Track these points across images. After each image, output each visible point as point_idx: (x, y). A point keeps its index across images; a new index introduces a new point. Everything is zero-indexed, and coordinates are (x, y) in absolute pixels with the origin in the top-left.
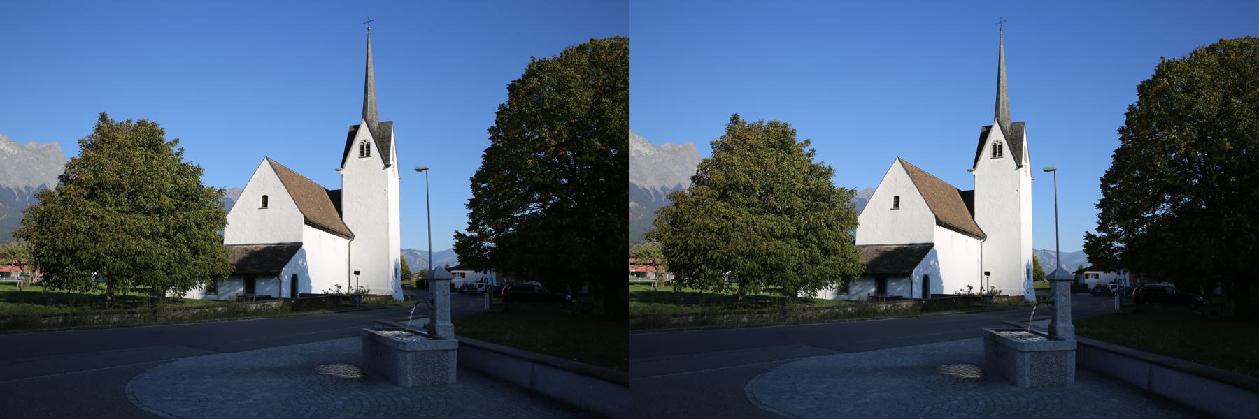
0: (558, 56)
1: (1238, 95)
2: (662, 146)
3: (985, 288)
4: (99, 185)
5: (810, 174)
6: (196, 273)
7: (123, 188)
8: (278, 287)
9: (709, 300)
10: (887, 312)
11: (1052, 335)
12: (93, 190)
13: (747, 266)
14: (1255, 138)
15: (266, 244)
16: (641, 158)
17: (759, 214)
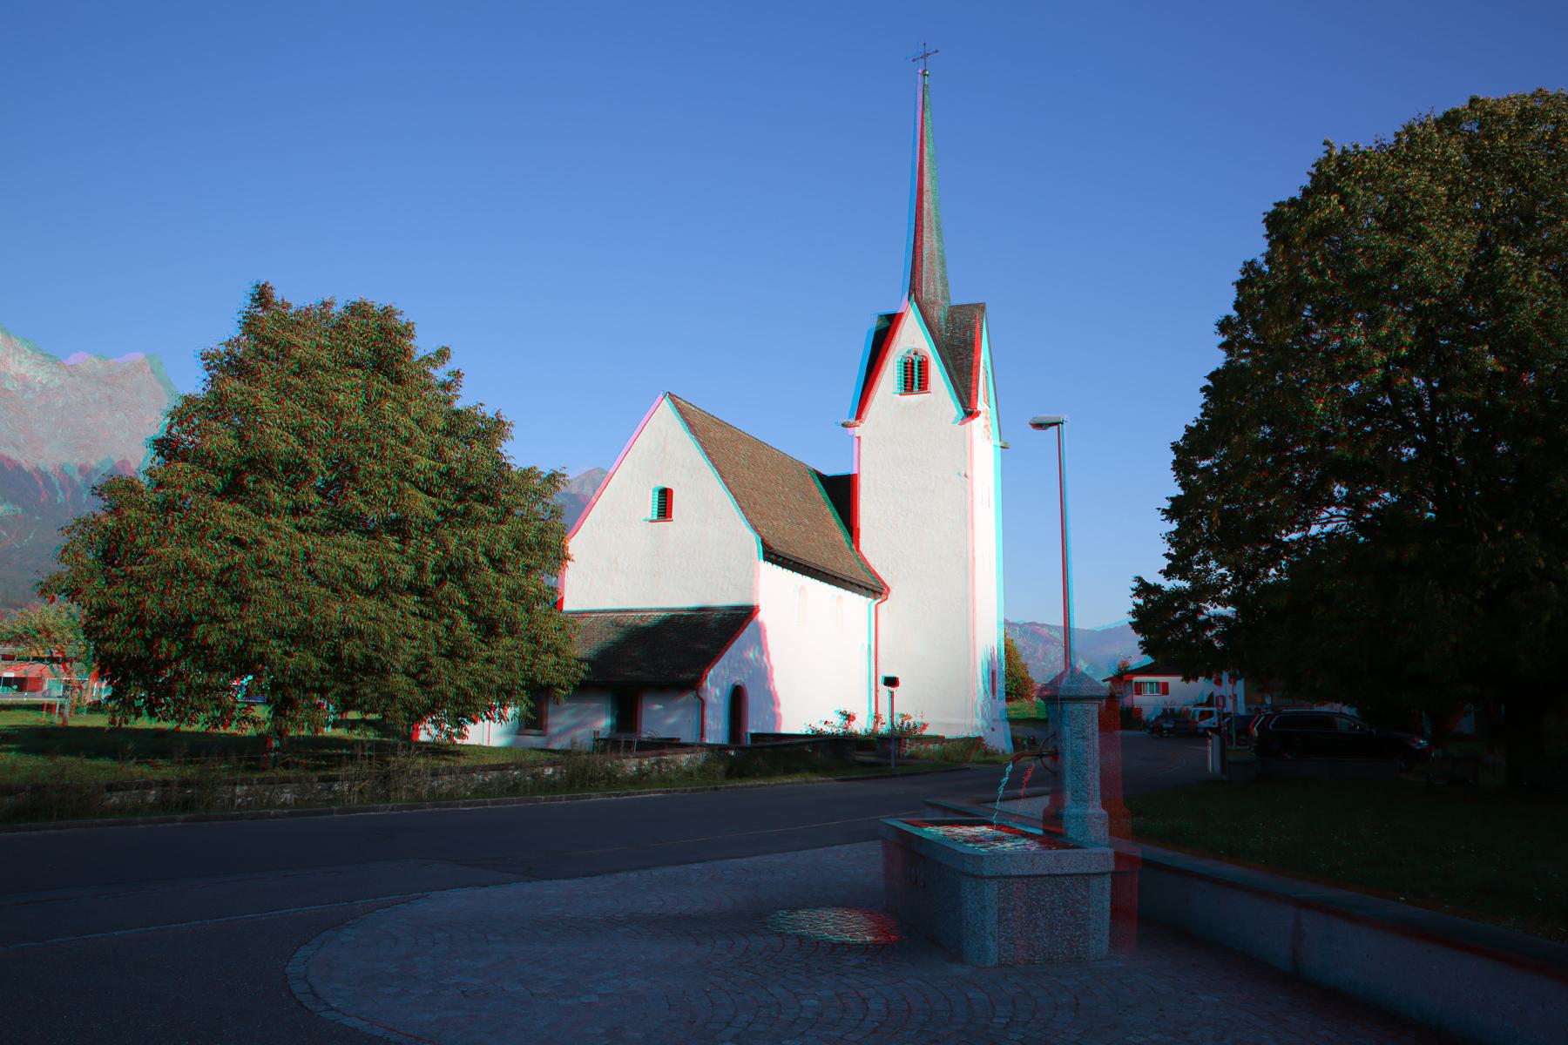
0: (1390, 140)
1: (1514, 236)
2: (65, 361)
3: (886, 718)
4: (251, 462)
5: (449, 434)
6: (492, 681)
7: (310, 473)
8: (695, 718)
9: (199, 748)
10: (641, 778)
11: (1054, 833)
12: (238, 474)
13: (292, 662)
14: (1558, 344)
16: (29, 396)
17: (322, 535)
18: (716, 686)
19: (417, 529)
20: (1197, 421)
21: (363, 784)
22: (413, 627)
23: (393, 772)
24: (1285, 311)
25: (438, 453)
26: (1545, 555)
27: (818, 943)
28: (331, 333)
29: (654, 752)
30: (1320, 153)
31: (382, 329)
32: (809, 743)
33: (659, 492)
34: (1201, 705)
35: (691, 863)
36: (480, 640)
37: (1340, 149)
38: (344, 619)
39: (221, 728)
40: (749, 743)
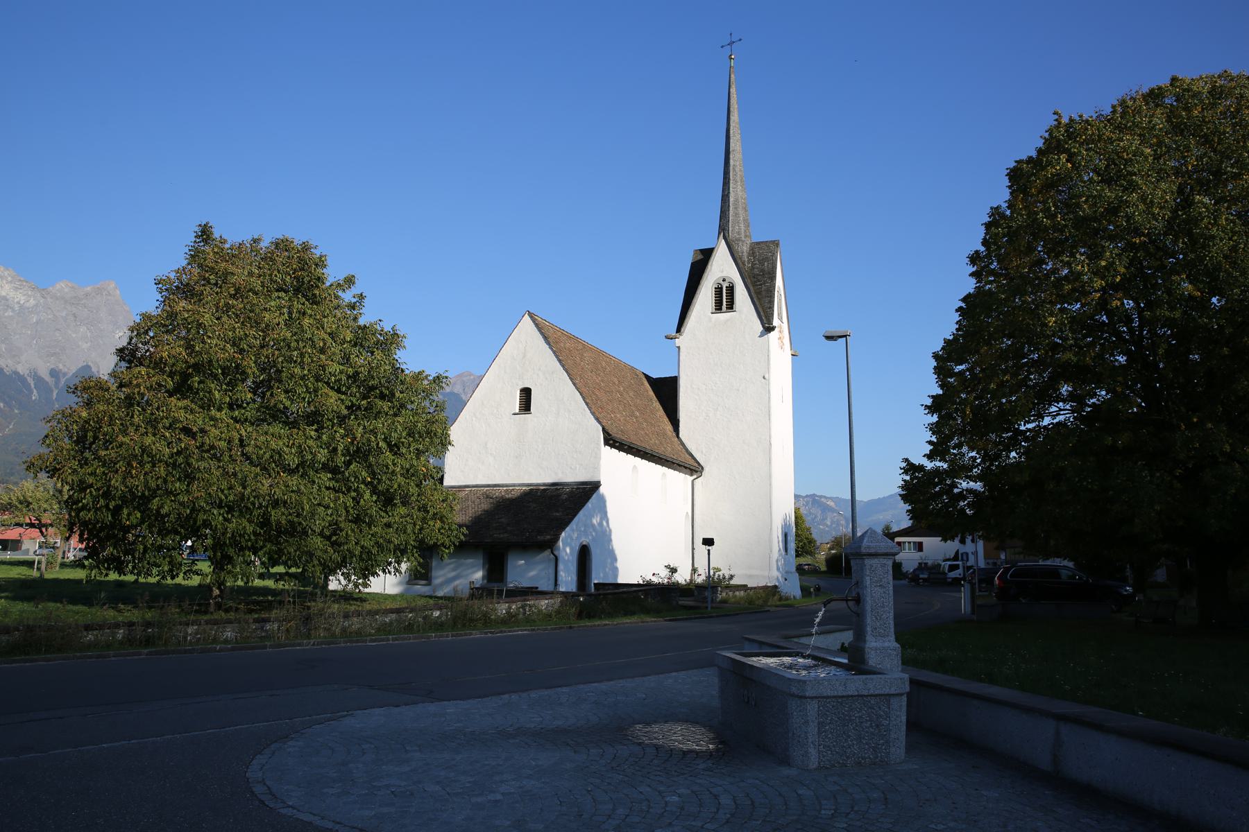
0: (1107, 110)
1: (1204, 186)
4: (197, 367)
6: (390, 542)
7: (244, 373)
8: (552, 571)
9: (159, 596)
10: (509, 620)
11: (856, 661)
12: (185, 377)
18: (567, 546)
19: (328, 420)
20: (954, 334)
21: (289, 624)
22: (327, 498)
23: (314, 614)
24: (1024, 246)
25: (346, 359)
26: (1230, 441)
27: (671, 751)
28: (260, 264)
29: (519, 598)
30: (1050, 121)
31: (300, 259)
32: (641, 591)
33: (521, 391)
34: (948, 560)
35: (560, 687)
36: (380, 509)
37: (1068, 118)
38: (271, 491)
39: (169, 578)
40: (593, 590)
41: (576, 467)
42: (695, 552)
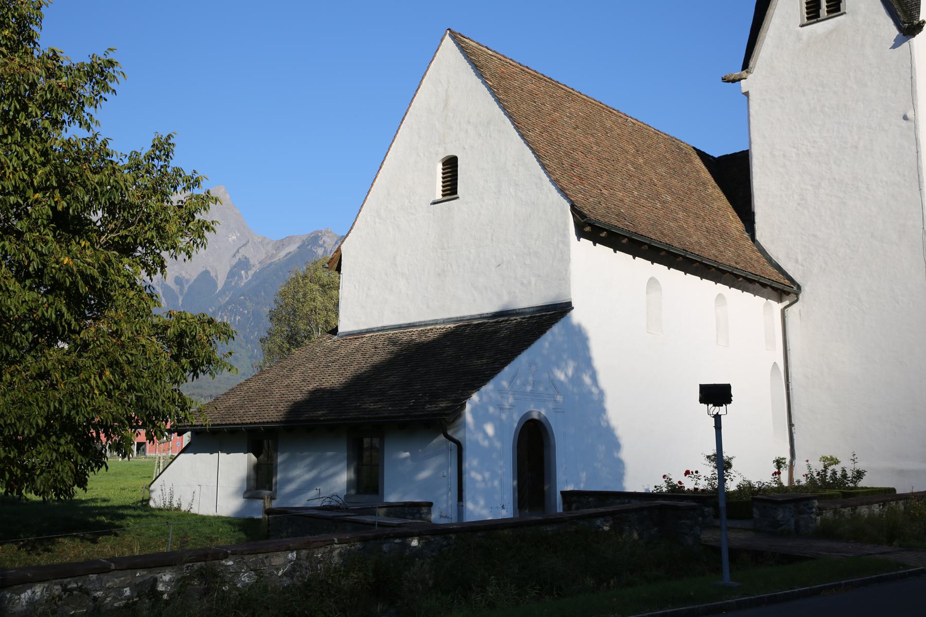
8: (453, 470)
15: (450, 321)
33: (444, 164)
40: (560, 509)
41: (530, 283)
42: (796, 430)
